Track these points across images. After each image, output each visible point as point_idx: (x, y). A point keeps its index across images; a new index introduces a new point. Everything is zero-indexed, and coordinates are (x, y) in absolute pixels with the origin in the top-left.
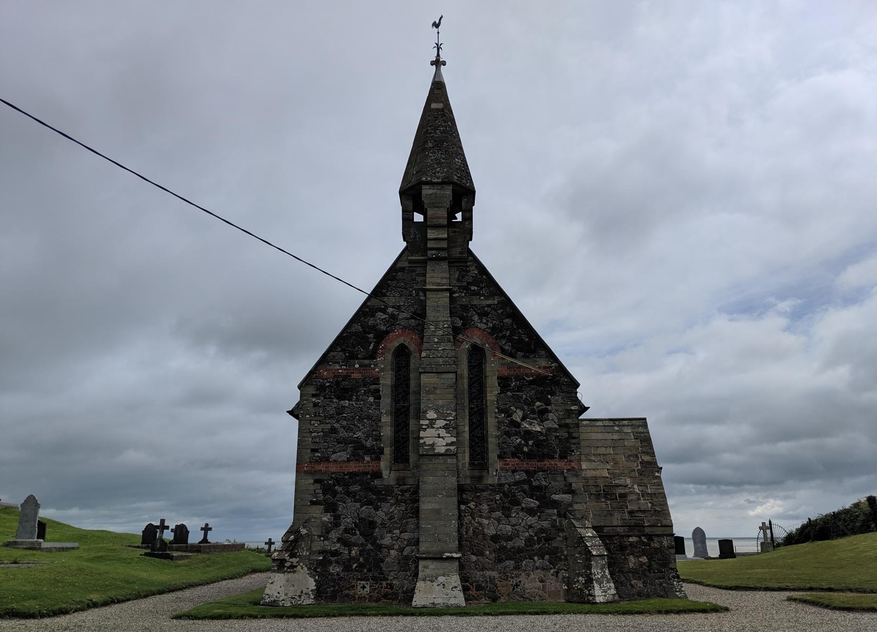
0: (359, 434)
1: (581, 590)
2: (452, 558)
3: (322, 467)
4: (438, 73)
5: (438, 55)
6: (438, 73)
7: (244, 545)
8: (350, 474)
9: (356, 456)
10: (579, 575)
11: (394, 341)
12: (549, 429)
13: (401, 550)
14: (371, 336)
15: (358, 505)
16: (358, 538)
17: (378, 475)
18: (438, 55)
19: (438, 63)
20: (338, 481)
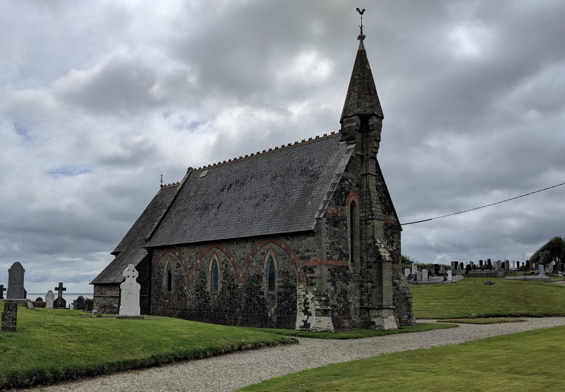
0: (341, 247)
1: (406, 321)
2: (390, 308)
3: (330, 262)
4: (362, 45)
5: (362, 32)
6: (362, 45)
7: (2, 313)
8: (339, 266)
9: (340, 259)
10: (404, 314)
11: (275, 293)
12: (394, 250)
13: (355, 305)
14: (343, 193)
15: (342, 282)
16: (342, 299)
17: (347, 268)
18: (362, 32)
19: (361, 38)
20: (335, 270)
